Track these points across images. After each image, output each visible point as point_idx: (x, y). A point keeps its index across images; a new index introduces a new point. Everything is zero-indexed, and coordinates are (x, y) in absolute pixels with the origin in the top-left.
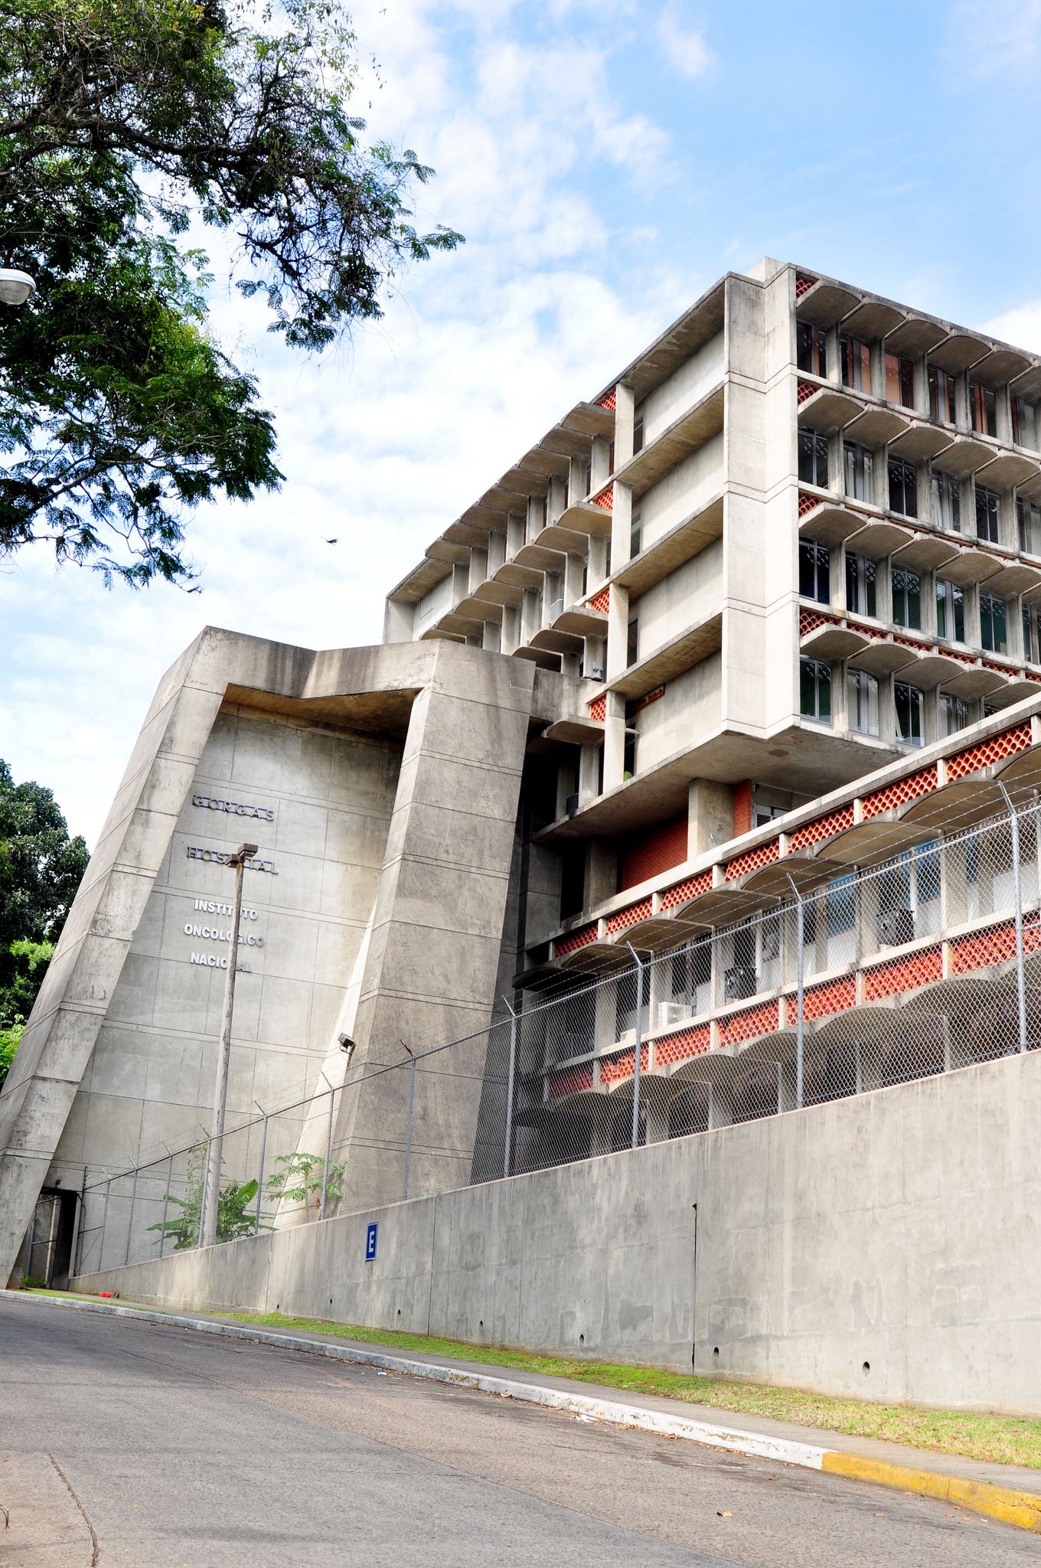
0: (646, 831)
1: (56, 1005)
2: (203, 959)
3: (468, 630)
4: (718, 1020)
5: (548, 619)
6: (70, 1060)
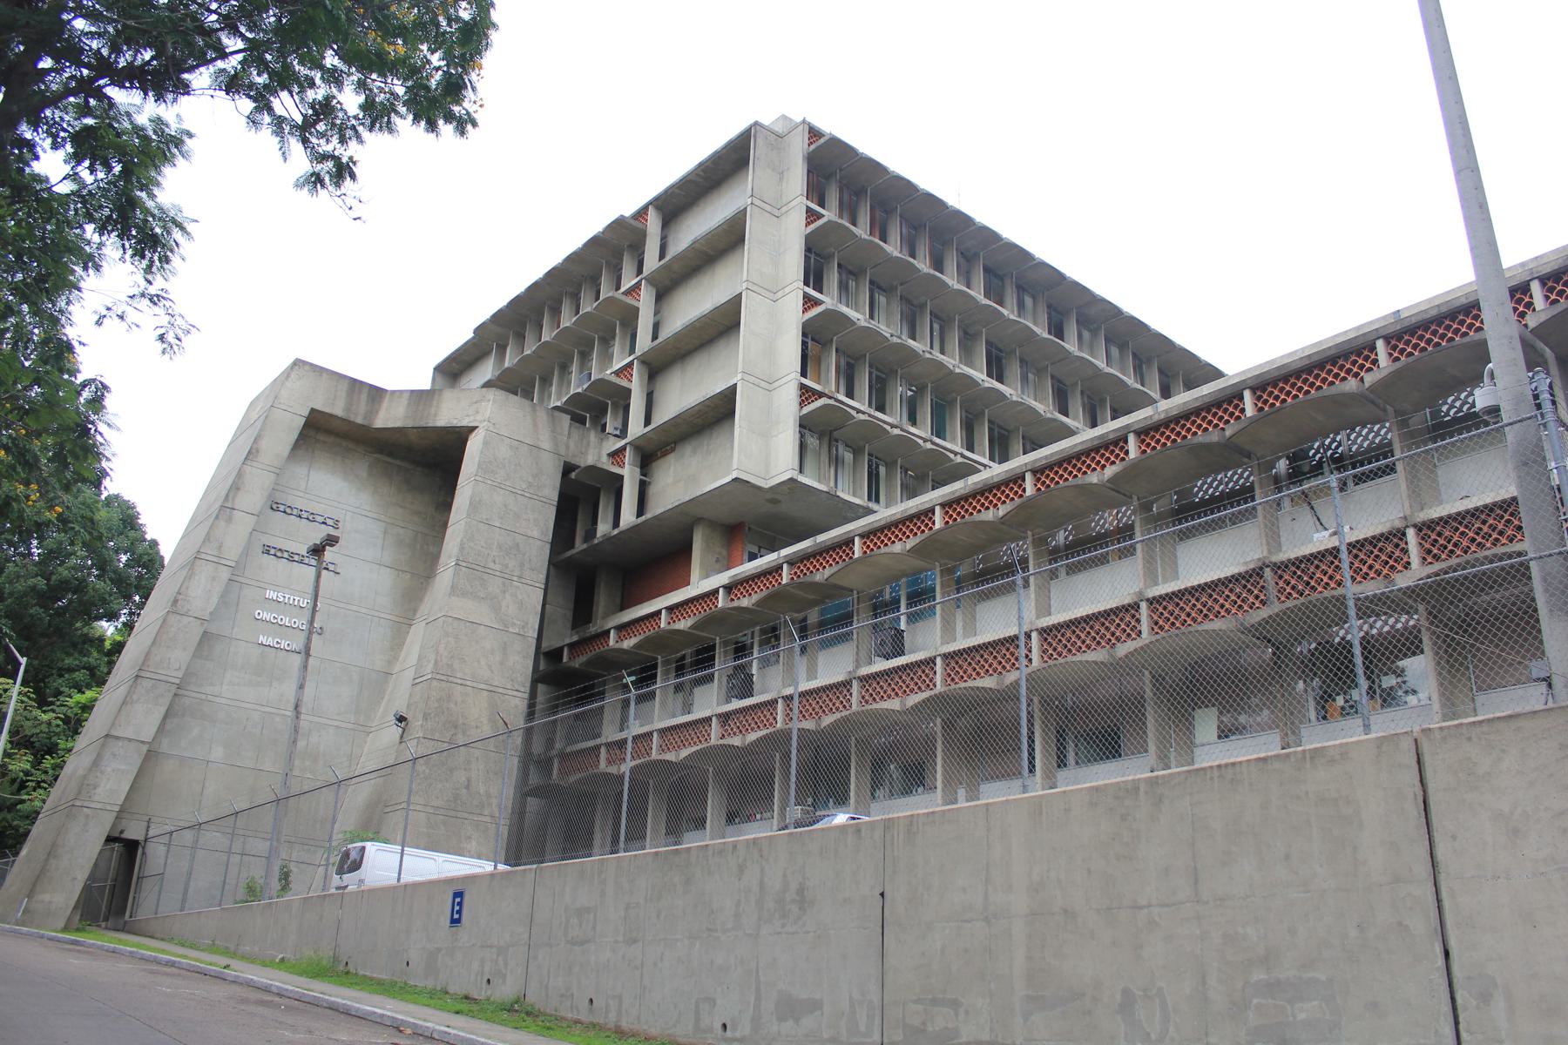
0: (658, 556)
1: (134, 672)
2: (270, 641)
3: (516, 384)
4: (719, 716)
5: (576, 387)
6: (144, 721)
